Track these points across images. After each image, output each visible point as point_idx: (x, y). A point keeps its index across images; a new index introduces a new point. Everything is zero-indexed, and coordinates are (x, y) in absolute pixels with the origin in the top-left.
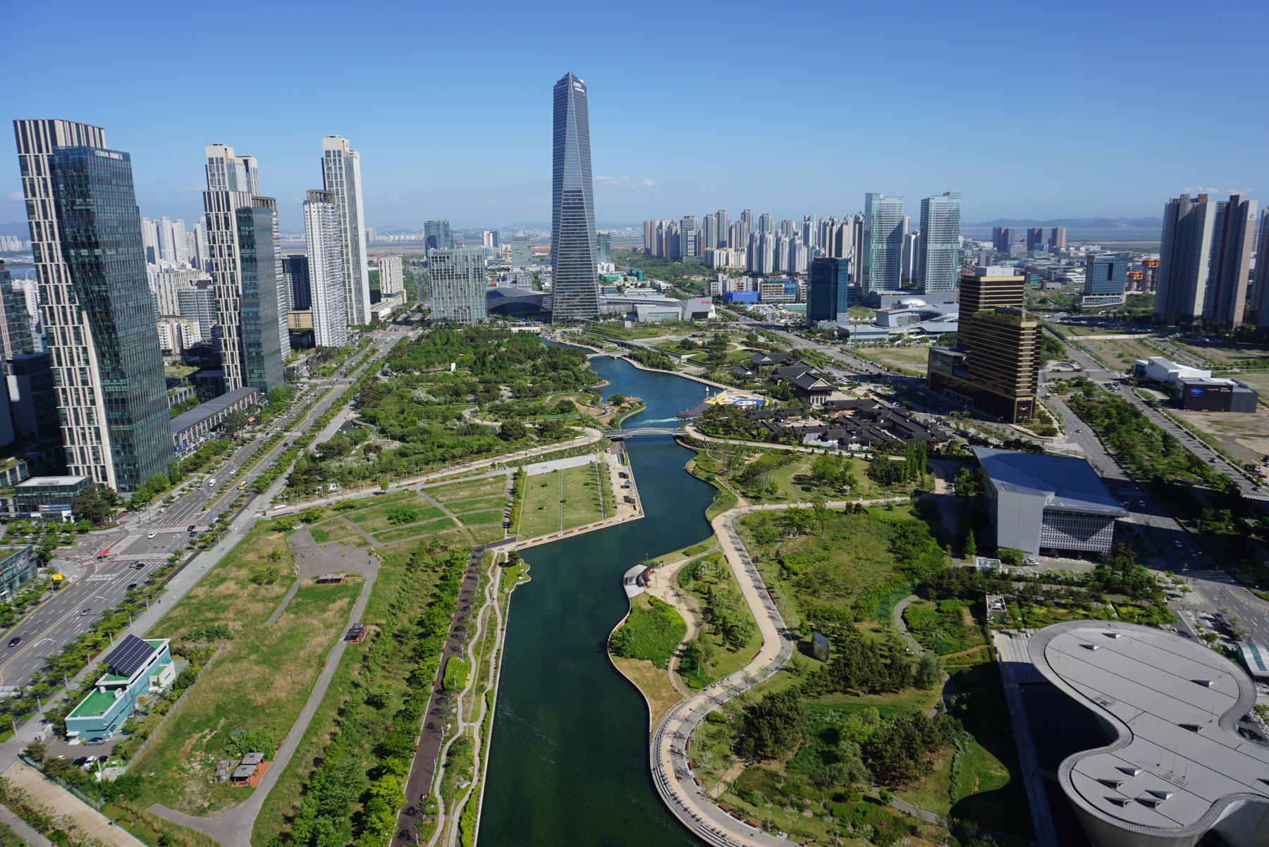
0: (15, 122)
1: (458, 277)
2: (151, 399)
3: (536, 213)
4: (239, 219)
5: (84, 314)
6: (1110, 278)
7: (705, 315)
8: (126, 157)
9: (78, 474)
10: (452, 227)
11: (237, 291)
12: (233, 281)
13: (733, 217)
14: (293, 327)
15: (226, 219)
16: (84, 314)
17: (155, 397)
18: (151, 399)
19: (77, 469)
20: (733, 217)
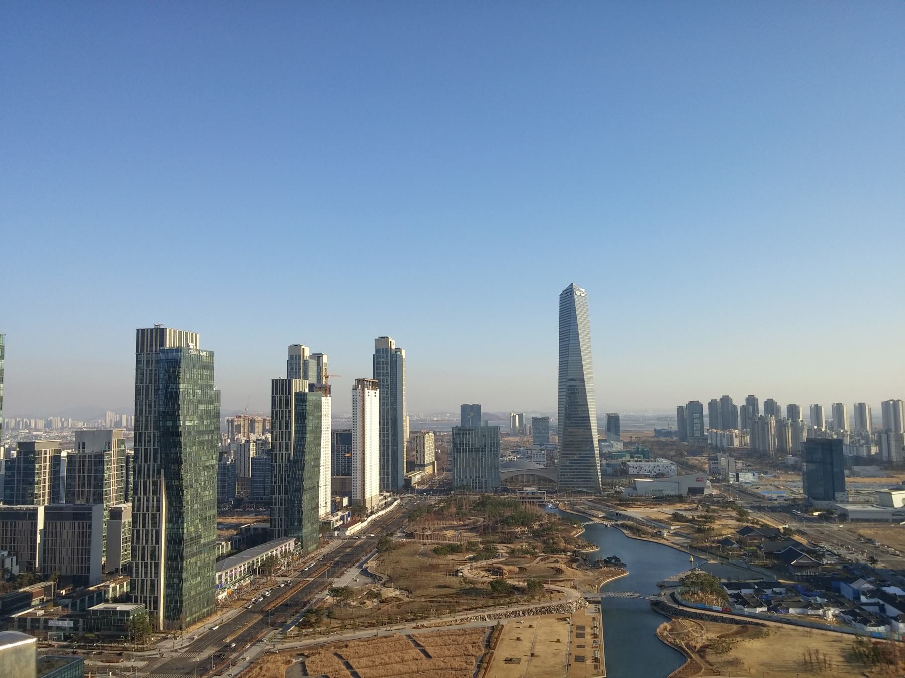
0: (138, 330)
1: (477, 450)
2: (202, 541)
3: (546, 401)
4: (296, 400)
5: (163, 470)
6: (567, 300)
7: (701, 490)
8: (211, 354)
9: (136, 602)
10: (483, 410)
11: (289, 457)
12: (286, 450)
13: (739, 402)
14: (214, 512)
15: (287, 400)
16: (163, 470)
17: (207, 540)
18: (202, 541)
19: (136, 597)
20: (739, 402)
